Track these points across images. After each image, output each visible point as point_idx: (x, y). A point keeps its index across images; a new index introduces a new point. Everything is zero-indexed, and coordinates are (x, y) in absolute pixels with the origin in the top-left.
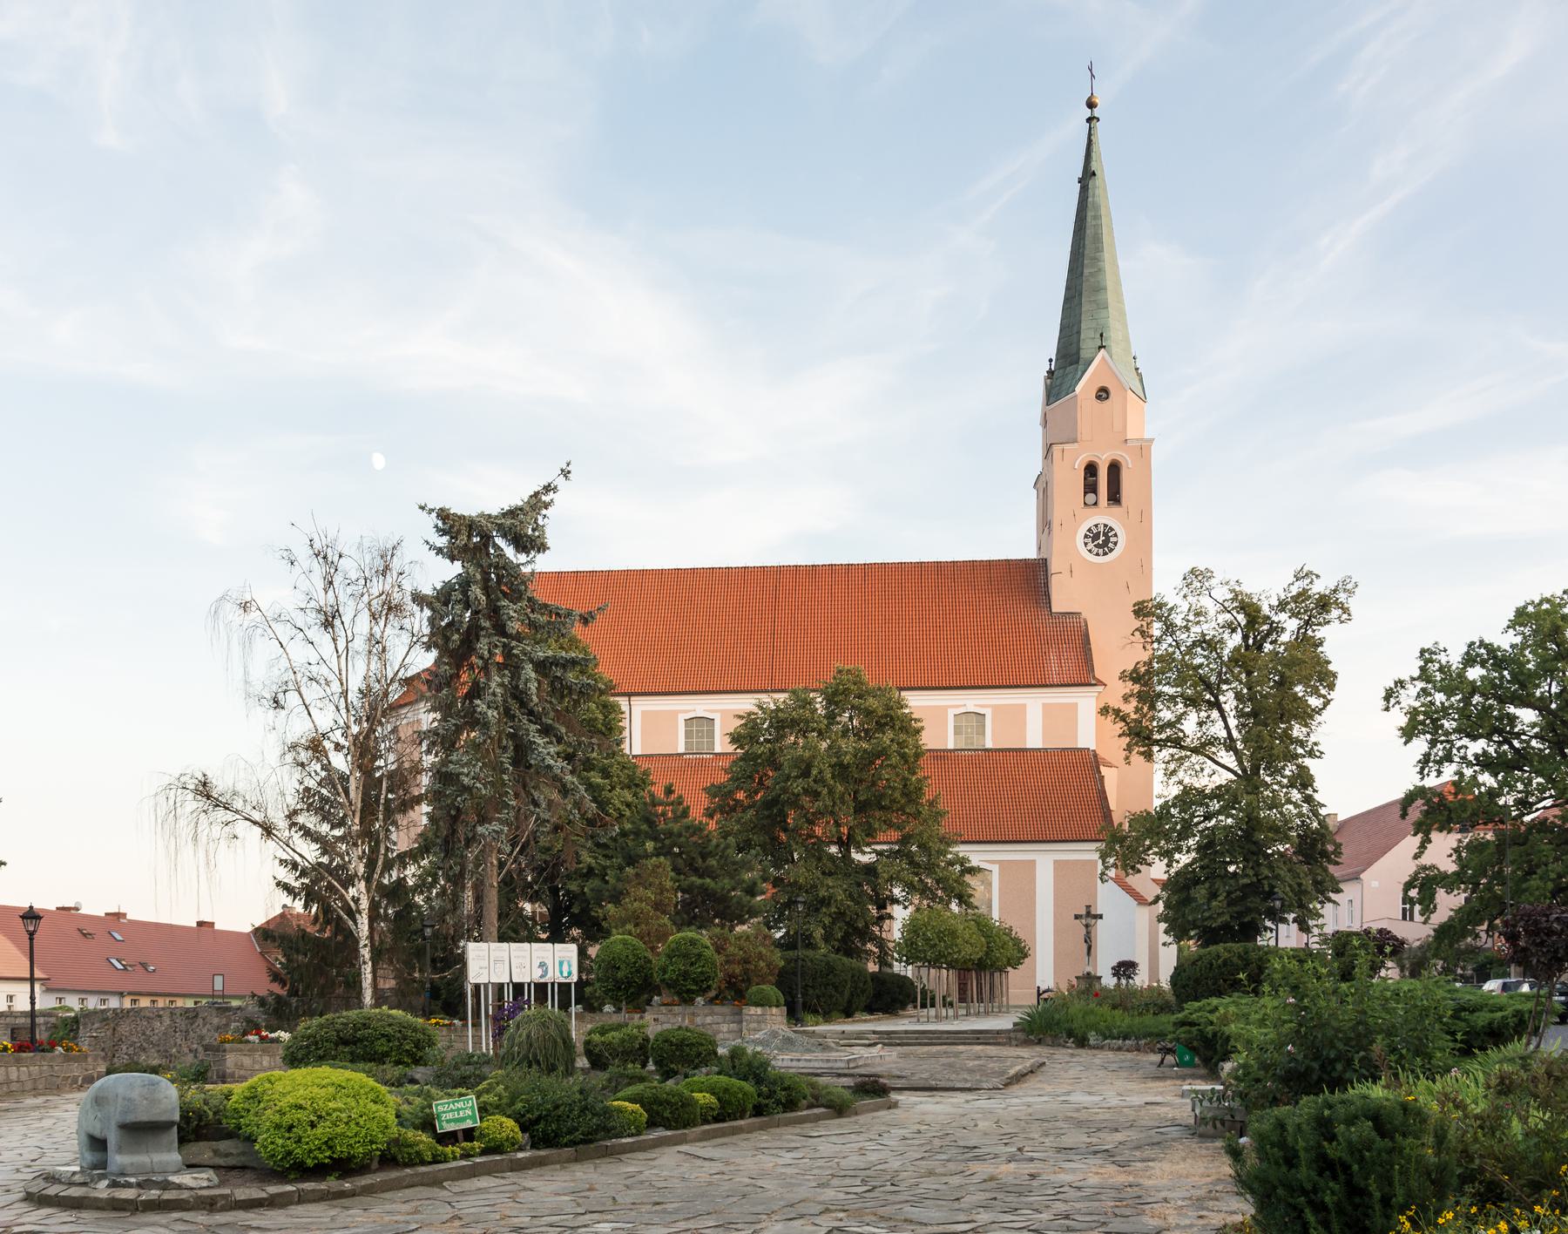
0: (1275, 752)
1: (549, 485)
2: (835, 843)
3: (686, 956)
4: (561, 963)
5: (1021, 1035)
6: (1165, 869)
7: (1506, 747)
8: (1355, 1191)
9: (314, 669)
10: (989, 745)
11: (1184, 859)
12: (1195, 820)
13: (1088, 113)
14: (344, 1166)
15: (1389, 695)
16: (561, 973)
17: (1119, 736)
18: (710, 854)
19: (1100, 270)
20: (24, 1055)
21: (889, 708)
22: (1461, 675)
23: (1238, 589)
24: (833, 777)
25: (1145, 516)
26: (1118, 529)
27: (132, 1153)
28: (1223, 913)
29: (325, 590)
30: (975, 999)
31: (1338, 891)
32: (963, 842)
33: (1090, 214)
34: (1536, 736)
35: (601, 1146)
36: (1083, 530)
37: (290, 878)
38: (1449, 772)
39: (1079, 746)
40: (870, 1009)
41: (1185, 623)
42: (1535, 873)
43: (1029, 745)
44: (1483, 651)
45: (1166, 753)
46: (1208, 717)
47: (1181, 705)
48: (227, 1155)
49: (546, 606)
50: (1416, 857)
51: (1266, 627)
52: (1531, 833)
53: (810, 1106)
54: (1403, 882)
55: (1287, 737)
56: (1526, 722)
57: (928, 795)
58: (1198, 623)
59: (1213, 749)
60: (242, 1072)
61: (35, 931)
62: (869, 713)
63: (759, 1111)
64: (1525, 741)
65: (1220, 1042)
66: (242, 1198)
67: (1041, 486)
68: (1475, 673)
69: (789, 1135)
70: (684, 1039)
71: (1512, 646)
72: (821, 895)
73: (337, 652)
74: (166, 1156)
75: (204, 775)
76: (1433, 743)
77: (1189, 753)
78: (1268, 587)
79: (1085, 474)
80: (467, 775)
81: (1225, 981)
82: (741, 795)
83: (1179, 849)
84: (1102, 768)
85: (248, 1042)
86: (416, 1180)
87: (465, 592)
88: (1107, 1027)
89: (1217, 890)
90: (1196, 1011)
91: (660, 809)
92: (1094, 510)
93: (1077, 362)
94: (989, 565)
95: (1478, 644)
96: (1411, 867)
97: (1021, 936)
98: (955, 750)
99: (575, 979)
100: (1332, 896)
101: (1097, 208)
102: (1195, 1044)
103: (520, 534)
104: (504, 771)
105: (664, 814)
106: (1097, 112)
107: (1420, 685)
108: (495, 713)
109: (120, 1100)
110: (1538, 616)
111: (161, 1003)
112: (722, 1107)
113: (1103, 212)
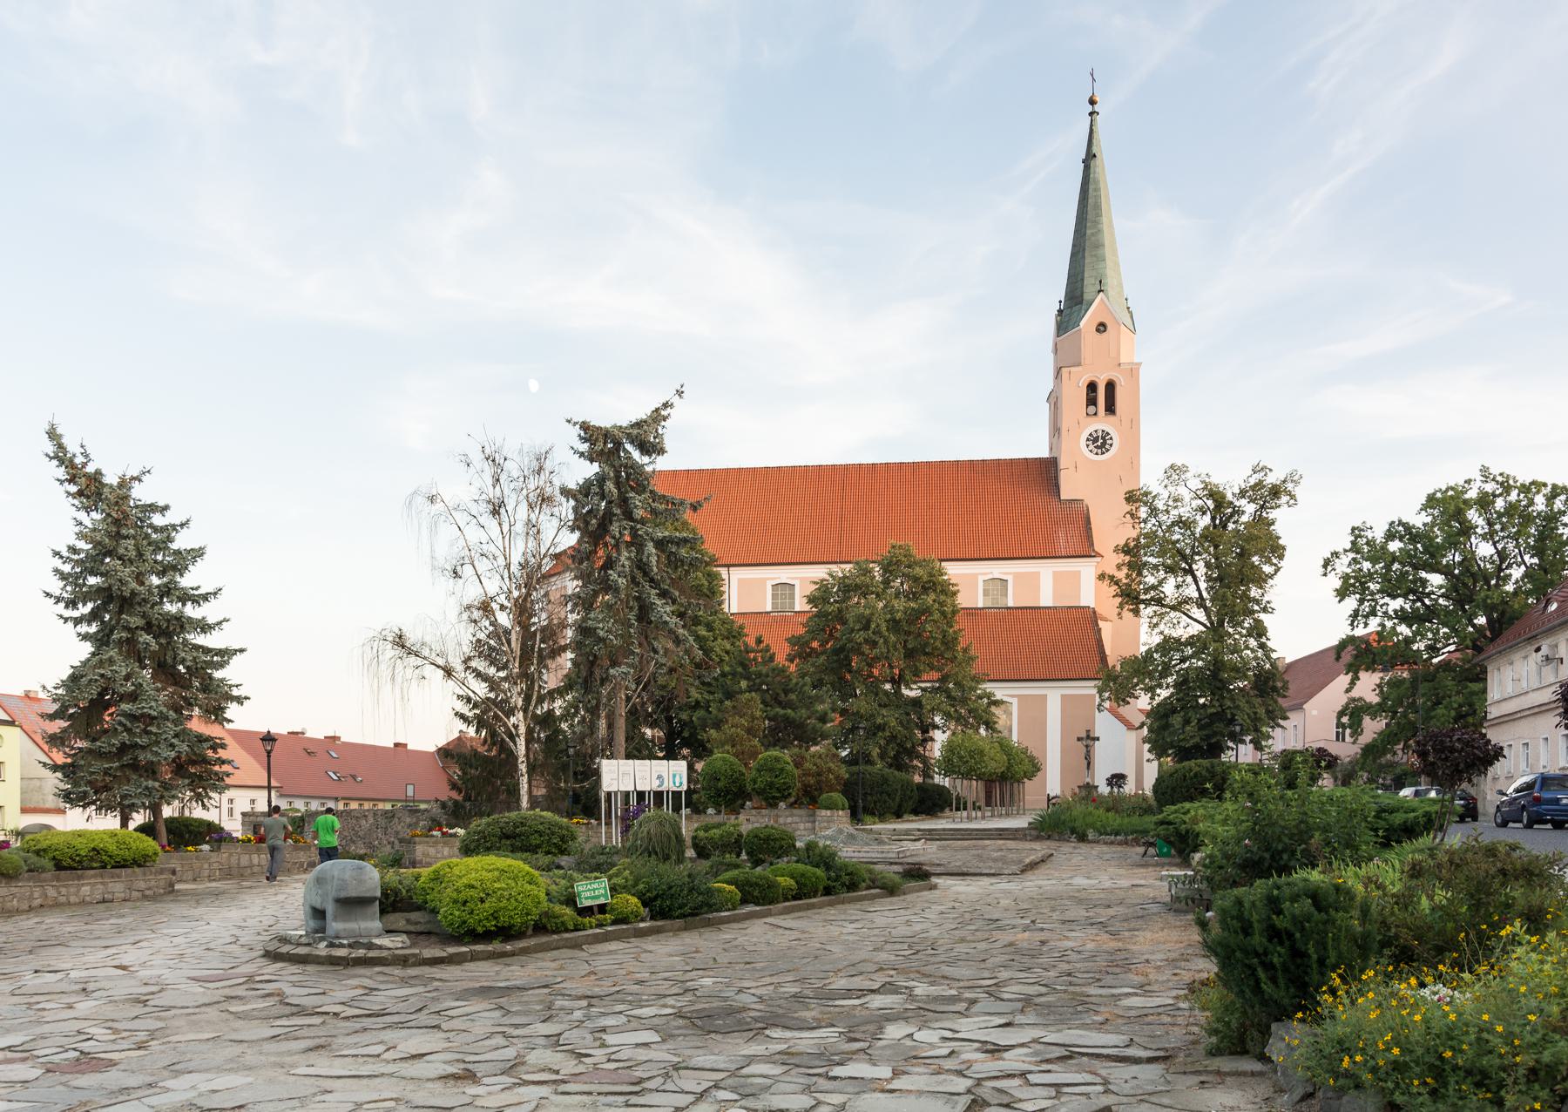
2: (889, 682)
3: (771, 770)
4: (674, 776)
5: (1034, 833)
7: (1419, 604)
8: (1297, 954)
9: (485, 547)
10: (1010, 604)
11: (1164, 693)
12: (1173, 663)
13: (1090, 109)
14: (506, 933)
15: (1327, 563)
16: (674, 783)
18: (792, 691)
19: (1100, 231)
21: (931, 575)
22: (1384, 547)
23: (1207, 480)
24: (888, 630)
25: (1134, 423)
26: (1113, 433)
27: (344, 921)
31: (1286, 718)
32: (989, 681)
33: (1091, 187)
34: (1442, 596)
35: (705, 919)
36: (1085, 435)
37: (465, 709)
38: (1374, 624)
40: (916, 812)
43: (1042, 604)
44: (1401, 528)
45: (1150, 610)
46: (1184, 581)
47: (1162, 572)
48: (416, 923)
49: (664, 496)
50: (1348, 691)
51: (1230, 510)
53: (869, 888)
55: (1246, 597)
58: (1176, 507)
59: (1188, 607)
60: (428, 860)
61: (271, 750)
62: (916, 579)
63: (828, 891)
66: (429, 956)
67: (1053, 400)
68: (1395, 546)
69: (852, 910)
71: (1424, 525)
74: (370, 924)
76: (1361, 601)
78: (1232, 479)
81: (1196, 789)
82: (815, 644)
83: (1160, 686)
84: (1099, 622)
85: (433, 836)
86: (561, 943)
87: (601, 487)
88: (1102, 826)
90: (1172, 813)
91: (752, 655)
92: (1094, 418)
93: (1081, 303)
94: (1012, 462)
96: (1344, 700)
98: (983, 608)
99: (685, 788)
101: (1097, 182)
102: (1172, 839)
104: (631, 626)
105: (755, 659)
106: (1097, 108)
108: (624, 581)
109: (335, 880)
110: (1444, 501)
111: (367, 806)
113: (1102, 185)
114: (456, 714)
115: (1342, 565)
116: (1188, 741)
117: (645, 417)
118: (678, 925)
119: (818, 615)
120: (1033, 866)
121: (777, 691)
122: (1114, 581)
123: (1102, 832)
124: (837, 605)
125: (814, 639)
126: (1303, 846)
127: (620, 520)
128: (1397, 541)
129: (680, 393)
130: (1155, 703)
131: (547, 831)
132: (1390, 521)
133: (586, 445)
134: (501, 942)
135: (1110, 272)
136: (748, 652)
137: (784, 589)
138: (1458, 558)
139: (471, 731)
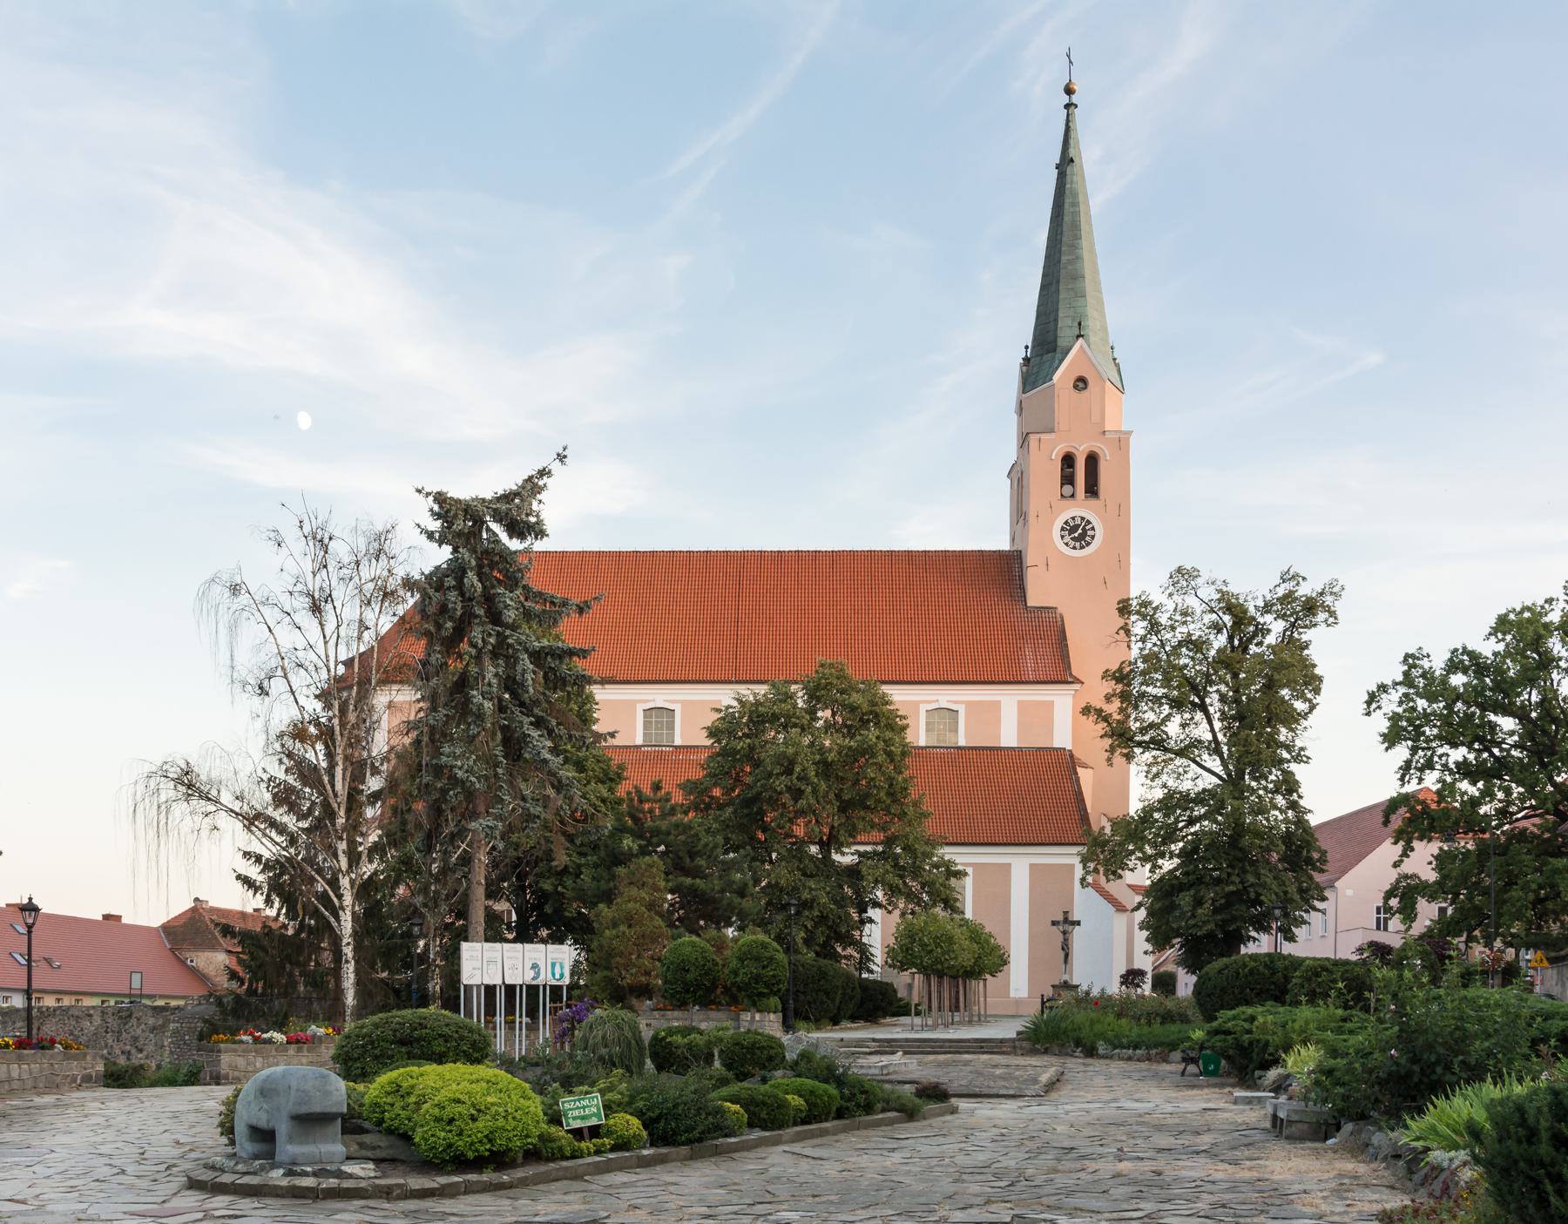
0: (1263, 756)
1: (544, 469)
2: (815, 843)
3: (757, 959)
4: (553, 965)
6: (1148, 874)
7: (1485, 755)
9: (301, 654)
10: (962, 742)
11: (1167, 865)
12: (1181, 825)
13: (1066, 99)
14: (498, 1159)
15: (1372, 698)
16: (553, 975)
17: (1101, 737)
18: (698, 854)
19: (1078, 258)
20: (26, 1052)
21: (873, 703)
22: (1444, 681)
23: (1225, 589)
24: (817, 775)
25: (1123, 510)
26: (1096, 522)
27: (301, 1143)
28: (1208, 921)
29: (313, 573)
30: (947, 1008)
31: (1324, 899)
32: (947, 844)
33: (1068, 201)
35: (712, 1145)
36: (1059, 523)
37: (254, 872)
38: (1431, 780)
39: (1002, 745)
40: (853, 1018)
41: (1170, 623)
42: (1516, 884)
43: (1003, 744)
44: (1465, 657)
45: (1148, 756)
46: (1192, 719)
47: (1166, 707)
48: (374, 1148)
49: (541, 594)
50: (1396, 865)
51: (1252, 628)
52: (1512, 844)
53: (884, 1110)
54: (1384, 890)
55: (1273, 743)
56: (1505, 729)
57: (914, 793)
58: (1185, 623)
60: (236, 1074)
61: (33, 924)
62: (853, 709)
63: (840, 1114)
64: (1505, 750)
65: (1256, 1050)
66: (417, 1187)
67: (1016, 476)
68: (1458, 680)
69: (876, 1137)
70: (754, 1043)
71: (1496, 654)
72: (803, 898)
73: (325, 637)
74: (332, 1147)
75: (188, 763)
76: (1414, 750)
77: (1173, 756)
78: (1255, 587)
79: (1062, 465)
80: (460, 768)
81: (1252, 990)
82: (717, 792)
83: (1162, 856)
84: (1079, 770)
85: (242, 1042)
86: (561, 1173)
88: (1115, 1036)
89: (1203, 897)
90: (1229, 1020)
91: (647, 806)
94: (962, 555)
95: (1461, 651)
96: (1392, 876)
97: (1000, 942)
99: (567, 981)
100: (1317, 904)
101: (1075, 195)
102: (1231, 1052)
103: (517, 520)
104: (497, 765)
105: (651, 811)
106: (1075, 99)
107: (1402, 690)
108: (490, 705)
110: (1520, 625)
112: (810, 1110)
113: (1081, 199)
114: (239, 877)
115: (1391, 703)
116: (1201, 927)
117: (515, 488)
118: (684, 1152)
119: (724, 753)
120: (1051, 1086)
121: (681, 854)
122: (1102, 716)
123: (1116, 1044)
124: (748, 741)
125: (715, 785)
126: (1461, 1058)
127: (482, 624)
128: (1460, 675)
129: (561, 458)
130: (1156, 877)
131: (456, 1036)
132: (1452, 648)
133: (438, 523)
134: (495, 1170)
135: (1091, 312)
136: (641, 801)
137: (659, 716)
138: (1535, 697)
139: (258, 901)
